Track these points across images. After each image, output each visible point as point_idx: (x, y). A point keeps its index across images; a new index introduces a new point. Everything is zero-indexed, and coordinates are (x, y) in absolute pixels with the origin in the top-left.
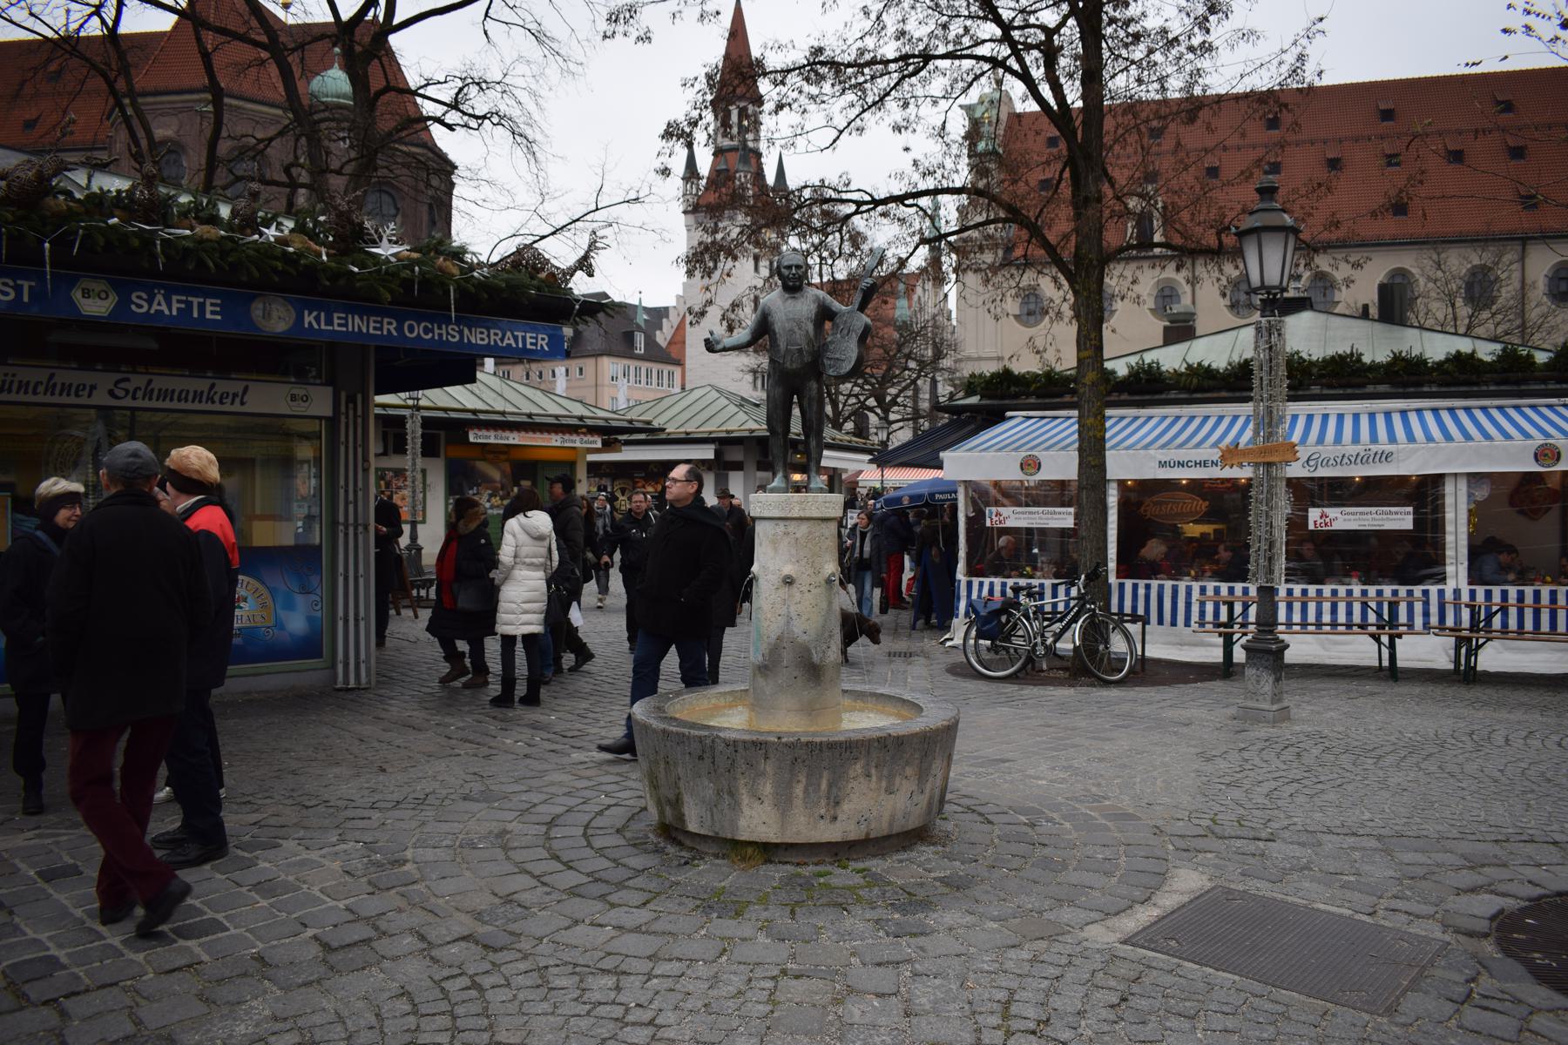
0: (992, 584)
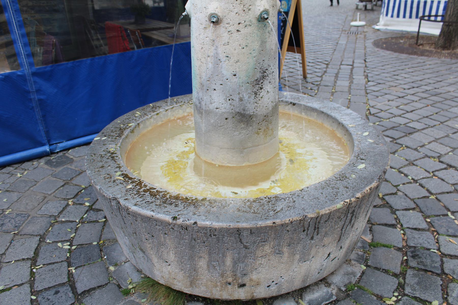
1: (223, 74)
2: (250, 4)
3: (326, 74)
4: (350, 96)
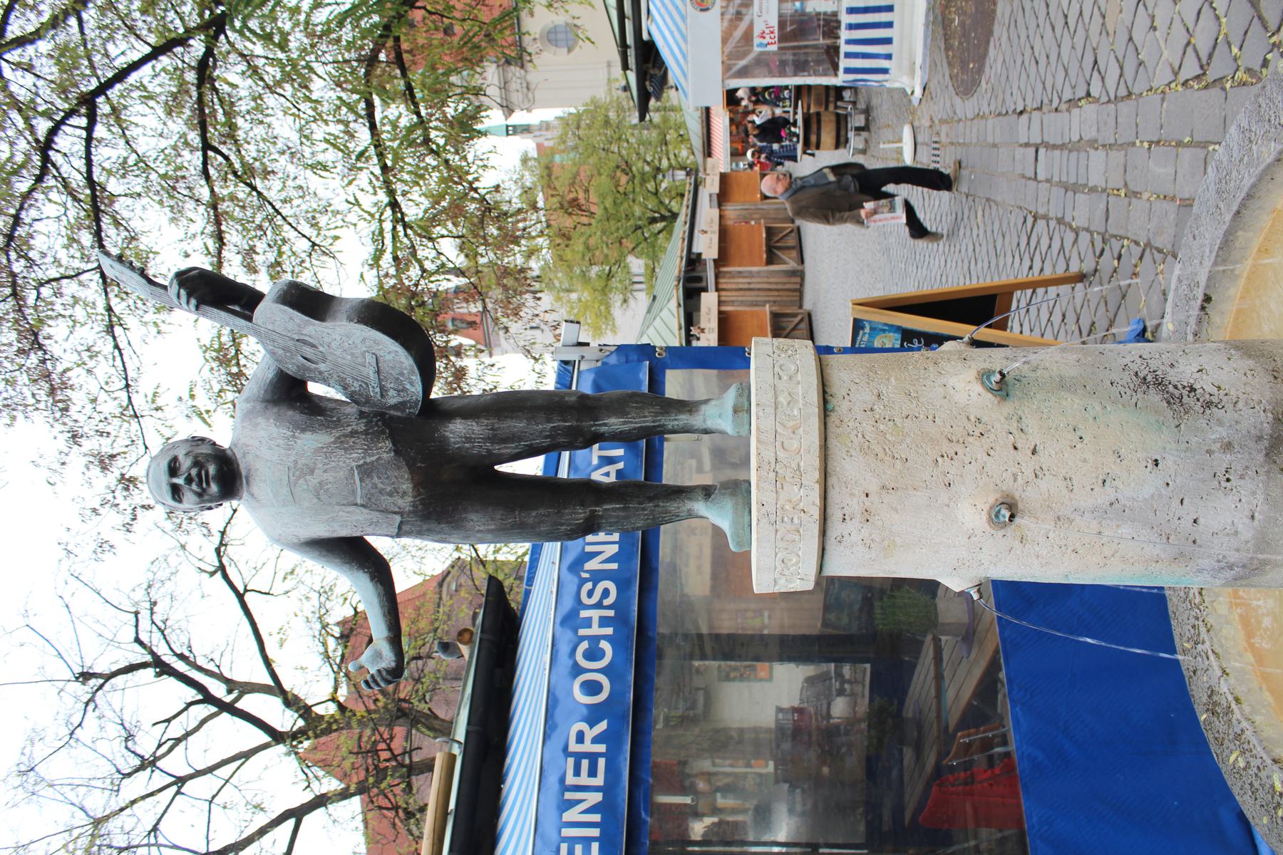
0: (849, 42)
1: (1153, 496)
2: (965, 419)
3: (1068, 219)
4: (1138, 143)
